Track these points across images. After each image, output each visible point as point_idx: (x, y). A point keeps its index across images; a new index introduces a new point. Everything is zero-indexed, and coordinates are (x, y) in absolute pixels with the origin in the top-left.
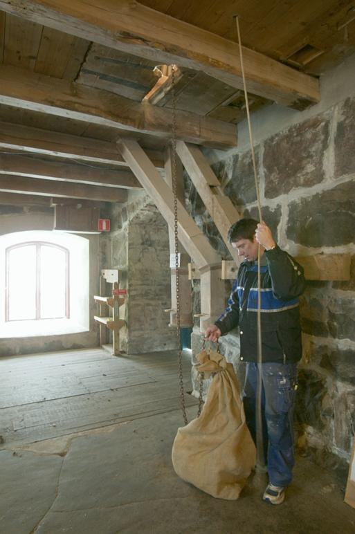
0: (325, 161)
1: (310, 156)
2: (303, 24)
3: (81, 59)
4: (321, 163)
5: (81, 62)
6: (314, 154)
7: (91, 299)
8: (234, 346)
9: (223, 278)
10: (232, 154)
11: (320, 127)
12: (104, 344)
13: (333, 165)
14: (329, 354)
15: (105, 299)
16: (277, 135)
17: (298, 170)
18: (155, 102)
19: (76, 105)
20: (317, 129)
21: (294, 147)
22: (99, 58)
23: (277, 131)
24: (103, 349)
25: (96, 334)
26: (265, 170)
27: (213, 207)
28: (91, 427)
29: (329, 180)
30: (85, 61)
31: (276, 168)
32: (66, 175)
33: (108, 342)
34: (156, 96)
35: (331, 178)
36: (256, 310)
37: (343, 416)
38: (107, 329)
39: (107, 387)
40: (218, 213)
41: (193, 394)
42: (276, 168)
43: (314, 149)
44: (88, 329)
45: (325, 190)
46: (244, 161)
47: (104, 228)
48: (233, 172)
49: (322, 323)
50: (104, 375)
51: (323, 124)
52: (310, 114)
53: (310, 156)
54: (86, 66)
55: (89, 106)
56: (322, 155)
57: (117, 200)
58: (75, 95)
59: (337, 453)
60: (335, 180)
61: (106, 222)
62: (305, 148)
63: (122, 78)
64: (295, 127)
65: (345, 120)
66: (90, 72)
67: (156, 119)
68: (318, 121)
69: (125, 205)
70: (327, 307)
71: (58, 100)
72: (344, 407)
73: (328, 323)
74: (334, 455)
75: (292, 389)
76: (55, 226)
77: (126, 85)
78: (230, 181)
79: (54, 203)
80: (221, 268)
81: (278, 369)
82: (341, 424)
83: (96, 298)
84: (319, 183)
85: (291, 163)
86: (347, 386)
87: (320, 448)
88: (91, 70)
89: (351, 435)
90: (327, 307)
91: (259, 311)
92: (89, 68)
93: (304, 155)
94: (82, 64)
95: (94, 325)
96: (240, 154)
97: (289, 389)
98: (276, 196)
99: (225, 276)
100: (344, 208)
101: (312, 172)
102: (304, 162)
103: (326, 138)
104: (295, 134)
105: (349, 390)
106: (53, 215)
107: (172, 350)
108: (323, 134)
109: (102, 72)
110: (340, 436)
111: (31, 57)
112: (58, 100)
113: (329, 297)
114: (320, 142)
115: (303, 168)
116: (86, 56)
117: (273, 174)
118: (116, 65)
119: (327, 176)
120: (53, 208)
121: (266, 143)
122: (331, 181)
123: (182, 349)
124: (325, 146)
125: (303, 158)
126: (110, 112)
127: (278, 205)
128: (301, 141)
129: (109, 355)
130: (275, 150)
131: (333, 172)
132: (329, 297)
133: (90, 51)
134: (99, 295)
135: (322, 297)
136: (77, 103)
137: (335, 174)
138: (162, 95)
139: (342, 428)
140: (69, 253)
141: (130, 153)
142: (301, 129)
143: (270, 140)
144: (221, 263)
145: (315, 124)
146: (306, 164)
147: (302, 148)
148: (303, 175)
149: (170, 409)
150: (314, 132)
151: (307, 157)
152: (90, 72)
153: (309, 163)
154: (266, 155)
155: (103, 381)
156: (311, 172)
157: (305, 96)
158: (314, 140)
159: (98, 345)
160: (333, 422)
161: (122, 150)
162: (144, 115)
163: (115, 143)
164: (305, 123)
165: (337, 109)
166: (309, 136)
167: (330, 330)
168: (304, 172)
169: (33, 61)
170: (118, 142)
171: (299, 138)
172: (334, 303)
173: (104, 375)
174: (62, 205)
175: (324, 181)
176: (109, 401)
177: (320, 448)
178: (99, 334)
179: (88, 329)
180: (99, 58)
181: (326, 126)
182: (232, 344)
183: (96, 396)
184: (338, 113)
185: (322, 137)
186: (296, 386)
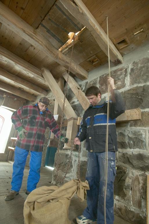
1: (119, 79)
2: (126, 29)
3: (43, 17)
4: (124, 81)
5: (42, 19)
7: (9, 138)
9: (78, 124)
12: (9, 160)
14: (128, 157)
16: (105, 74)
18: (63, 52)
19: (34, 37)
20: (122, 71)
22: (50, 20)
23: (105, 73)
24: (9, 162)
25: (7, 155)
26: (100, 85)
27: (78, 94)
29: (127, 87)
30: (44, 19)
31: (104, 84)
32: (15, 81)
34: (64, 49)
35: (128, 86)
37: (137, 188)
39: (7, 177)
40: (80, 96)
42: (104, 84)
43: (121, 77)
44: (4, 153)
45: (126, 90)
46: (91, 83)
49: (125, 142)
50: (7, 172)
51: (125, 69)
52: (120, 67)
54: (44, 23)
56: (125, 78)
59: (133, 210)
60: (130, 87)
63: (55, 35)
64: (113, 71)
66: (44, 26)
67: (62, 58)
68: (123, 69)
70: (128, 135)
72: (138, 183)
73: (128, 142)
74: (132, 212)
76: (2, 104)
77: (55, 39)
79: (5, 95)
80: (77, 120)
81: (111, 156)
82: (136, 192)
83: (9, 147)
84: (123, 88)
86: (139, 172)
87: (124, 208)
88: (45, 25)
89: (142, 198)
90: (128, 135)
91: (108, 124)
93: (117, 79)
94: (42, 20)
95: (7, 150)
98: (104, 94)
99: (79, 123)
100: (135, 95)
101: (120, 84)
102: (117, 81)
104: (113, 73)
105: (139, 174)
106: (3, 101)
108: (125, 72)
109: (48, 28)
110: (136, 200)
111: (22, 8)
113: (128, 131)
114: (123, 75)
116: (45, 16)
117: (103, 86)
118: (56, 26)
119: (127, 85)
120: (4, 98)
121: (100, 77)
122: (128, 87)
123: (45, 166)
124: (126, 75)
127: (105, 97)
128: (115, 75)
129: (11, 165)
131: (129, 84)
133: (48, 14)
135: (125, 131)
136: (35, 36)
137: (130, 84)
138: (67, 49)
139: (136, 194)
140: (4, 120)
144: (78, 118)
145: (121, 70)
146: (118, 82)
152: (44, 26)
153: (119, 81)
154: (100, 80)
157: (119, 59)
160: (130, 192)
164: (117, 69)
169: (22, 11)
170: (42, 69)
171: (115, 74)
172: (131, 133)
173: (7, 172)
174: (8, 97)
175: (125, 87)
176: (8, 183)
177: (124, 208)
178: (8, 155)
179: (4, 153)
180: (50, 20)
181: (126, 70)
185: (124, 73)
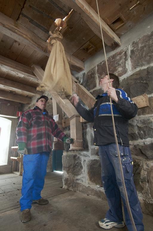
0: (127, 65)
1: (119, 65)
4: (125, 66)
6: (121, 64)
8: (87, 157)
9: (81, 121)
10: (82, 73)
11: (122, 54)
13: (131, 66)
15: (16, 158)
16: (103, 61)
17: (114, 71)
20: (121, 55)
21: (112, 63)
25: (11, 166)
28: (4, 211)
29: (129, 72)
30: (23, 7)
31: (104, 73)
33: (17, 170)
35: (130, 71)
36: (111, 115)
38: (17, 162)
39: (15, 189)
41: (63, 187)
43: (121, 62)
45: (128, 76)
47: (19, 115)
48: (83, 79)
49: (135, 133)
50: (14, 184)
51: (124, 53)
52: (118, 50)
53: (119, 65)
54: (24, 12)
55: (22, 33)
56: (125, 63)
57: (27, 103)
58: (16, 27)
61: (17, 148)
62: (117, 63)
64: (111, 56)
65: (134, 48)
69: (30, 105)
71: (7, 25)
75: (130, 164)
77: (41, 29)
78: (82, 83)
83: (12, 158)
85: (111, 69)
92: (25, 13)
95: (10, 161)
96: (86, 72)
97: (129, 164)
102: (117, 67)
103: (126, 57)
107: (49, 172)
112: (7, 25)
114: (123, 59)
115: (117, 70)
119: (129, 70)
123: (53, 171)
124: (126, 59)
125: (116, 66)
126: (32, 39)
129: (17, 176)
130: (103, 66)
131: (131, 69)
132: (136, 120)
134: (13, 156)
136: (17, 30)
137: (132, 69)
141: (38, 70)
142: (114, 57)
143: (100, 64)
145: (120, 53)
146: (118, 68)
147: (115, 63)
148: (117, 72)
149: (53, 195)
150: (120, 56)
151: (118, 65)
152: (25, 16)
155: (13, 186)
156: (121, 71)
158: (121, 58)
159: (11, 172)
161: (33, 69)
162: (47, 47)
163: (30, 67)
164: (116, 54)
165: (129, 46)
166: (118, 58)
167: (139, 136)
168: (117, 71)
173: (14, 184)
175: (127, 72)
176: (17, 195)
178: (12, 166)
181: (126, 53)
182: (85, 156)
183: (9, 193)
184: (130, 47)
185: (124, 57)
186: (133, 162)
